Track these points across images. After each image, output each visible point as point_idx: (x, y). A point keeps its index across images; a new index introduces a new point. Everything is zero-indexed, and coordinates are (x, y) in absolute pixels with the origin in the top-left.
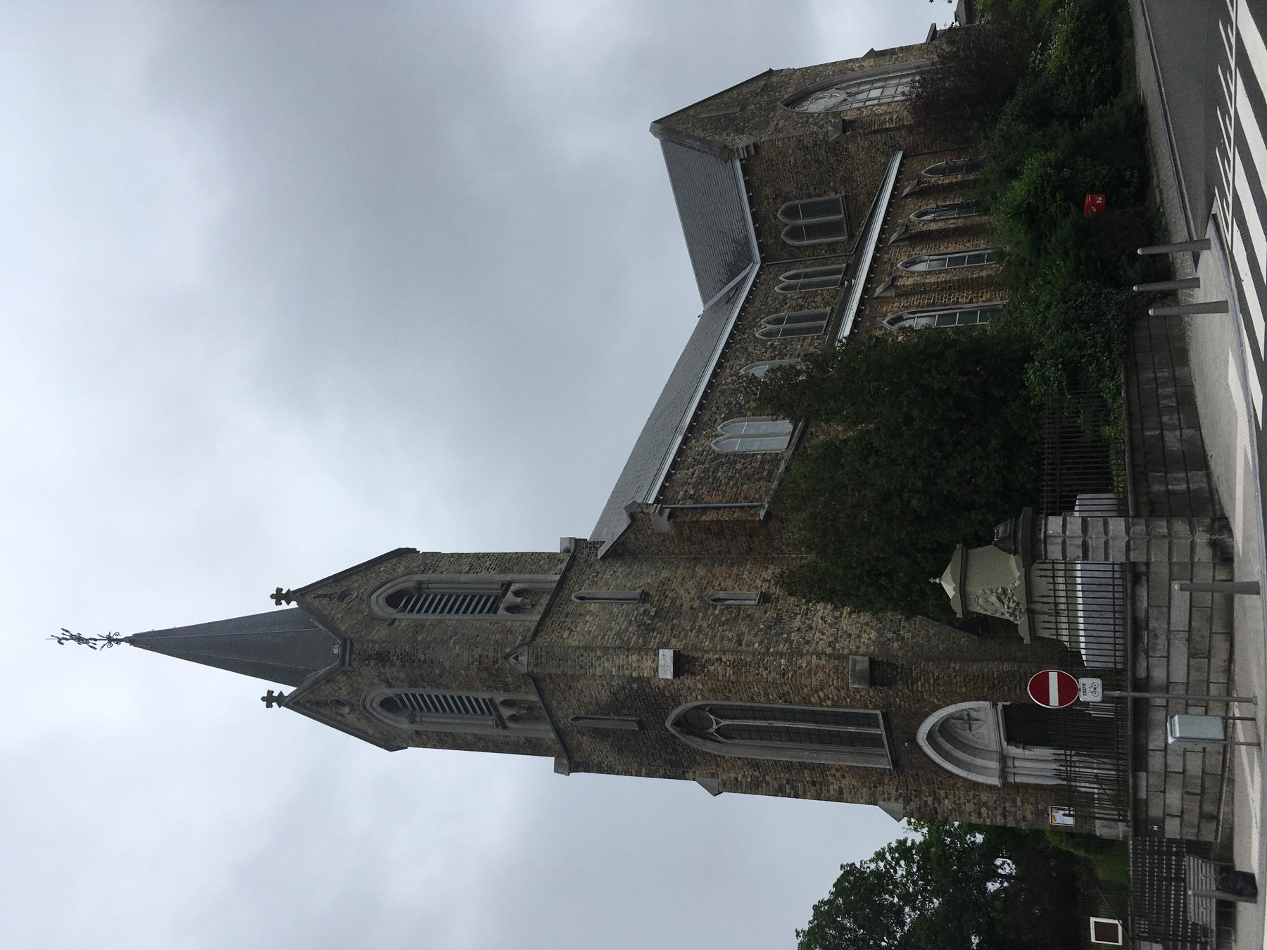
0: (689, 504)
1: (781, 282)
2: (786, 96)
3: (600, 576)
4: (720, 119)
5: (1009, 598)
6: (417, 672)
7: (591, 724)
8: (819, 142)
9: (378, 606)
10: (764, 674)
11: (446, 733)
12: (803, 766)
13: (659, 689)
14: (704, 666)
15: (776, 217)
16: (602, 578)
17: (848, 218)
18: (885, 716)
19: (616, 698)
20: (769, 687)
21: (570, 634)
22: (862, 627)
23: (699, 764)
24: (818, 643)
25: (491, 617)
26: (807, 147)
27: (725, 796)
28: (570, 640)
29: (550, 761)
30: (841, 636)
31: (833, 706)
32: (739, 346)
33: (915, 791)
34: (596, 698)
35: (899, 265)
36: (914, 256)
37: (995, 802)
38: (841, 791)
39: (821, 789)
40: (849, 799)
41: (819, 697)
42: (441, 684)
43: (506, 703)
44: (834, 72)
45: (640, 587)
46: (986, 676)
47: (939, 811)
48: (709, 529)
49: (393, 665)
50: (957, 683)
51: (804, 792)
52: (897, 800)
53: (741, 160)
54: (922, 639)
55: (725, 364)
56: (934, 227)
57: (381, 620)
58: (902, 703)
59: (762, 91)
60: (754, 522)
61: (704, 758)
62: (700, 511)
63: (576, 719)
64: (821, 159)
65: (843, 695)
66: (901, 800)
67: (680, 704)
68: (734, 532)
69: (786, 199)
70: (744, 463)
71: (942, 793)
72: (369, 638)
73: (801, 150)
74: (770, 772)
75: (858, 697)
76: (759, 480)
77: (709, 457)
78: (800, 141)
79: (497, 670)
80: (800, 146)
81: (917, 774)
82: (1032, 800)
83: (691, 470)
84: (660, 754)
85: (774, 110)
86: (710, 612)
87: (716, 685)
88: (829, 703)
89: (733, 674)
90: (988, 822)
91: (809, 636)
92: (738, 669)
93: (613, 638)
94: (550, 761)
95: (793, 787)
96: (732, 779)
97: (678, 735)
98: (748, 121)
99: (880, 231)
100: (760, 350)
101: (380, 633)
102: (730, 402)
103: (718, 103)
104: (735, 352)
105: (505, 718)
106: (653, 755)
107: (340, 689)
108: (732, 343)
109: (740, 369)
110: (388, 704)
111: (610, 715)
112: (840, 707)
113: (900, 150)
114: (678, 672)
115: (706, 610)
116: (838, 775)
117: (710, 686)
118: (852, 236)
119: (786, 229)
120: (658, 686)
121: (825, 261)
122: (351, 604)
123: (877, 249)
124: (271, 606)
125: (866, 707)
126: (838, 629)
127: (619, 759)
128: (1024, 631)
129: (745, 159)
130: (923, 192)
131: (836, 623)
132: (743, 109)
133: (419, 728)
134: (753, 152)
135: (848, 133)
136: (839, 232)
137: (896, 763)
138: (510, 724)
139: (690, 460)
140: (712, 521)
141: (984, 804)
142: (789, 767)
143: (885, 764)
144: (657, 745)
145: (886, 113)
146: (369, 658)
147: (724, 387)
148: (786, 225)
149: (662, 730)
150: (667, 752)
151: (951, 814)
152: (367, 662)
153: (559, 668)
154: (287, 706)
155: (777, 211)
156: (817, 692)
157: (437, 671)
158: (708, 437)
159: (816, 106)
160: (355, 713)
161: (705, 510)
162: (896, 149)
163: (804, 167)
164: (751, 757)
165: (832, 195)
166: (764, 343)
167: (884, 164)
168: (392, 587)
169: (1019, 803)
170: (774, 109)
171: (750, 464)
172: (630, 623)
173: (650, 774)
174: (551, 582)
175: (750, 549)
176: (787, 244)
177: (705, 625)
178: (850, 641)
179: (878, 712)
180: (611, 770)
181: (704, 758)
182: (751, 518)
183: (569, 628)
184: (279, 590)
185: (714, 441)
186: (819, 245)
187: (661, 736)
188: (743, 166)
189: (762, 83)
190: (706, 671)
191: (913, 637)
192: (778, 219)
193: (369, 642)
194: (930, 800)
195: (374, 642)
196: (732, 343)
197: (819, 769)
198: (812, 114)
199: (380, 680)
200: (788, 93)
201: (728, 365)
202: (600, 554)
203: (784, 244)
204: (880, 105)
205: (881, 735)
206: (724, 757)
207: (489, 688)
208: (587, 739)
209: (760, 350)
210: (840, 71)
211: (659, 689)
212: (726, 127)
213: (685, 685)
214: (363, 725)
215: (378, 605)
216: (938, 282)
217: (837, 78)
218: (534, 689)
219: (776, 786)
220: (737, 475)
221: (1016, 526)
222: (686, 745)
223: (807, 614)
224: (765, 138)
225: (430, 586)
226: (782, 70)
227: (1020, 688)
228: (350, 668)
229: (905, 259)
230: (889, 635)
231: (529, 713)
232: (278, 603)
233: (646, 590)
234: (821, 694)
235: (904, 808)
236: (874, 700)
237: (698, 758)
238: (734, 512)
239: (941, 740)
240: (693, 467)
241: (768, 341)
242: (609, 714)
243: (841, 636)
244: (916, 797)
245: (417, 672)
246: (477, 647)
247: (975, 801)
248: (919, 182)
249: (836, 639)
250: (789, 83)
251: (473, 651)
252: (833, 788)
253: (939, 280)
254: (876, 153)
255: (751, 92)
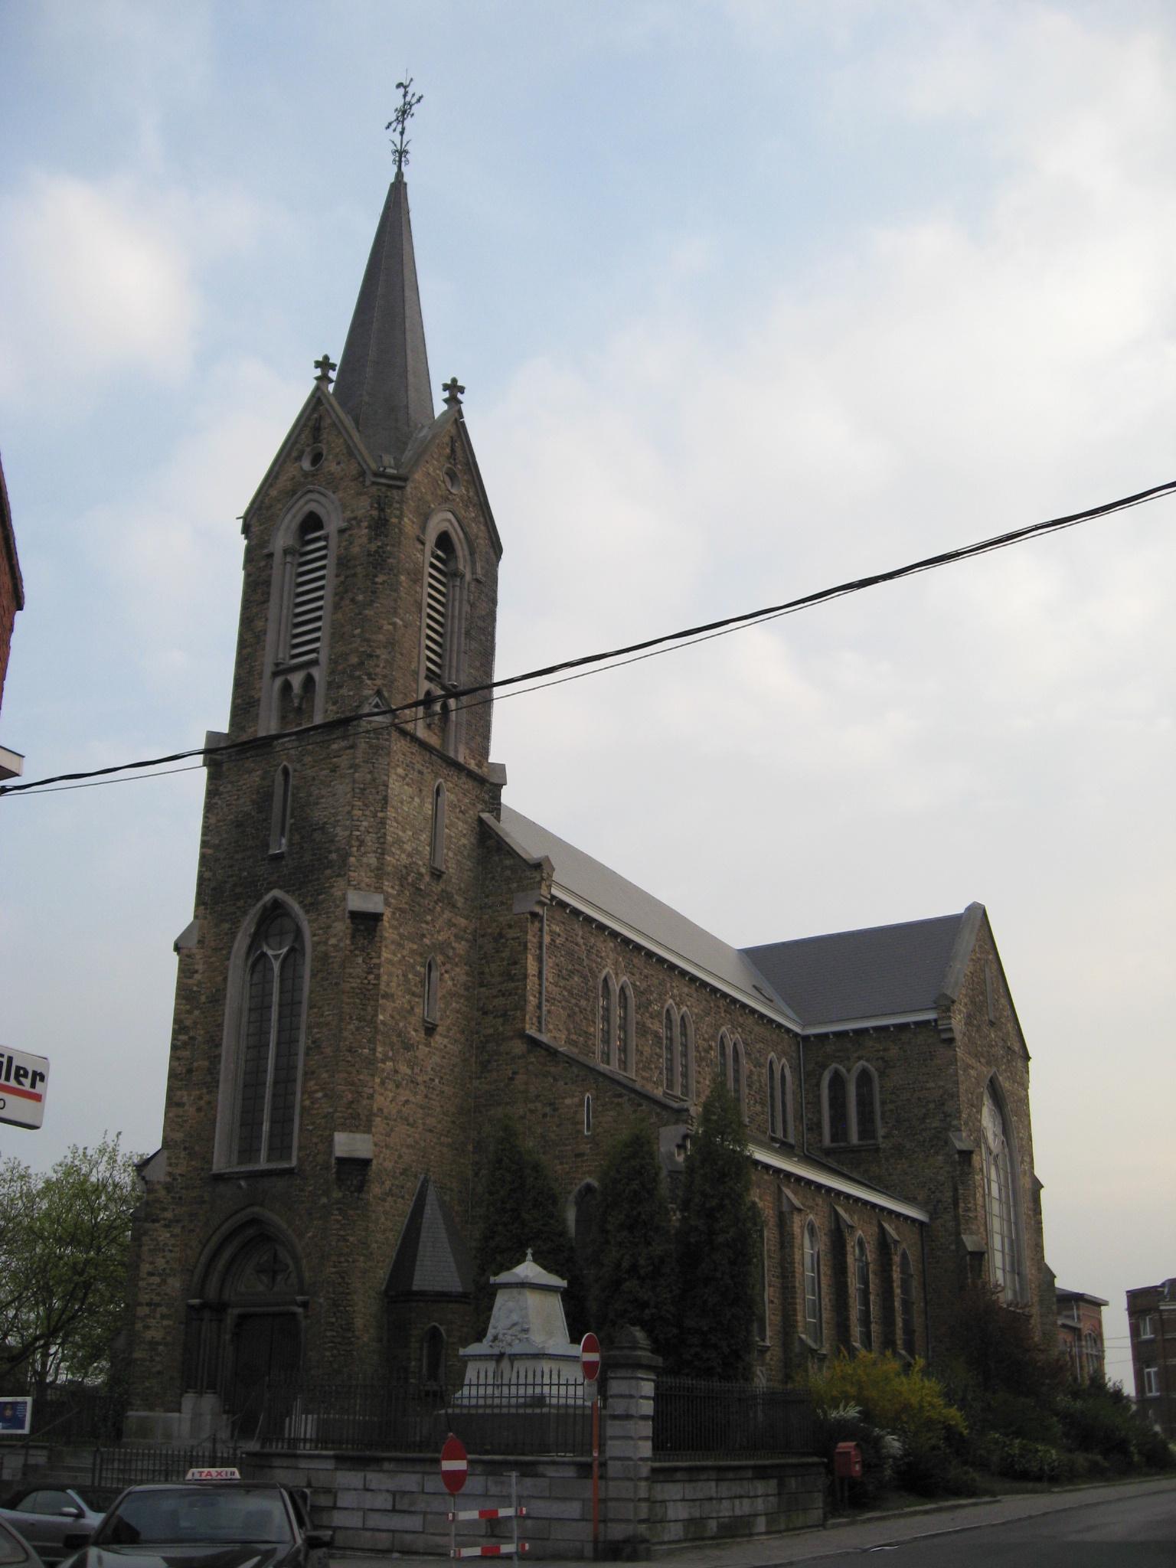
0: (547, 939)
1: (779, 1059)
2: (1000, 1078)
3: (461, 815)
4: (982, 993)
5: (516, 1336)
6: (359, 569)
7: (279, 791)
8: (948, 1119)
9: (441, 521)
10: (352, 1027)
11: (268, 593)
12: (215, 1060)
13: (329, 887)
14: (363, 949)
15: (860, 1058)
16: (458, 818)
17: (854, 1150)
18: (289, 1172)
19: (315, 830)
20: (330, 1030)
21: (400, 776)
22: (396, 1150)
23: (217, 926)
24: (382, 1094)
25: (423, 673)
26: (943, 1104)
27: (175, 958)
28: (395, 777)
29: (224, 727)
30: (388, 1124)
31: (303, 1108)
32: (712, 1005)
33: (180, 1198)
34: (317, 804)
35: (811, 1216)
36: (819, 1234)
37: (166, 1294)
38: (180, 1105)
39: (181, 1080)
40: (170, 1115)
41: (316, 1091)
42: (342, 599)
43: (309, 681)
44: (1022, 1139)
45: (447, 868)
46: (349, 1297)
47: (157, 1225)
48: (515, 963)
49: (370, 541)
50: (340, 1262)
51: (179, 1059)
52: (170, 1174)
53: (936, 1020)
54: (383, 1224)
55: (694, 986)
56: (850, 1259)
57: (423, 528)
58: (307, 1194)
59: (1008, 1048)
60: (523, 1020)
61: (227, 934)
62: (538, 952)
63: (286, 772)
64: (928, 1121)
65: (318, 1122)
66: (168, 1179)
67: (307, 912)
68: (510, 994)
69: (882, 1074)
70: (585, 1010)
71: (177, 1230)
72: (406, 511)
73: (941, 1097)
74: (206, 1017)
75: (315, 1140)
76: (568, 1029)
77: (594, 965)
78: (952, 1097)
79: (359, 677)
80: (946, 1097)
81: (204, 1202)
82: (169, 1339)
83: (581, 941)
84: (232, 876)
85: (987, 1063)
86: (419, 959)
87: (333, 963)
88: (307, 1103)
89: (352, 988)
90: (142, 1284)
91: (390, 1085)
92: (357, 994)
93: (395, 833)
94: (224, 727)
95: (185, 1044)
96: (196, 967)
97: (260, 905)
98: (979, 1029)
99: (789, 1172)
100: (706, 1032)
101: (409, 524)
102: (651, 993)
103: (999, 991)
104: (706, 1001)
105: (289, 678)
106: (231, 866)
107: (338, 463)
108: (716, 996)
109: (687, 1006)
110: (312, 523)
111: (291, 818)
112: (301, 1116)
113: (931, 1219)
114: (356, 916)
115: (421, 955)
116: (202, 1103)
117: (333, 954)
118: (828, 1152)
119: (843, 1070)
120: (333, 886)
121: (799, 1118)
122: (443, 485)
123: (830, 1190)
124: (438, 378)
125: (300, 1148)
126: (395, 1120)
127: (225, 820)
128: (474, 1349)
129: (936, 1025)
130: (884, 1245)
131: (401, 1118)
132: (992, 1024)
133: (278, 559)
134: (944, 1036)
135: (957, 1156)
136: (834, 1139)
137: (219, 1178)
138: (279, 682)
139: (593, 940)
140: (526, 969)
141: (164, 1281)
142: (215, 1042)
143: (219, 1165)
144: (246, 874)
145: (975, 1204)
146: (381, 510)
147: (669, 985)
148: (849, 1071)
149: (268, 883)
150: (235, 885)
151: (152, 1240)
152: (376, 505)
153: (364, 762)
154: (317, 389)
155: (868, 1060)
156: (322, 1089)
157: (360, 598)
158: (616, 963)
159: (988, 1119)
160: (303, 476)
161: (540, 960)
162: (933, 1215)
163: (919, 1099)
164: (228, 996)
165: (881, 1131)
166: (713, 1037)
167: (915, 1199)
168: (459, 539)
169: (165, 1323)
170: (988, 1063)
171: (585, 1018)
172: (410, 855)
173: (204, 860)
174: (456, 751)
175: (485, 1013)
176: (824, 1070)
177: (405, 953)
178: (382, 1134)
179: (294, 1163)
180: (209, 808)
181: (227, 934)
182: (527, 1017)
183: (407, 775)
184: (462, 390)
185: (611, 971)
186: (819, 1112)
187: (259, 880)
188: (928, 1022)
189: (1017, 1047)
190: (357, 952)
191: (385, 1213)
192: (857, 1062)
193: (401, 509)
194: (168, 1215)
195: (400, 517)
196: (716, 996)
197: (210, 1080)
198: (980, 1112)
199: (349, 520)
200: (1006, 1085)
201: (693, 991)
202: (485, 816)
203: (824, 1067)
204: (984, 1196)
205: (257, 1161)
206: (228, 959)
207: (333, 662)
208: (255, 782)
209: (706, 1032)
210: (1022, 1146)
211: (329, 887)
212: (973, 1002)
213: (333, 922)
214: (283, 482)
215: (438, 523)
216: (794, 1263)
217: (1015, 1142)
218: (332, 717)
219: (188, 1023)
220: (573, 1001)
221: (645, 1349)
222: (245, 913)
223: (412, 1082)
224: (960, 1052)
225: (457, 589)
226: (1028, 1072)
227: (334, 1337)
228: (368, 483)
229: (817, 1225)
230: (388, 1184)
231: (293, 705)
232: (446, 387)
233: (445, 876)
234: (320, 1095)
235: (159, 1182)
236: (311, 1159)
237: (226, 926)
238: (535, 997)
239: (251, 1232)
240: (585, 944)
241: (716, 1042)
242: (292, 816)
243: (388, 1124)
244: (173, 1198)
245: (359, 569)
246: (390, 653)
247: (168, 1271)
248: (896, 1242)
249: (386, 1118)
250: (1014, 1082)
251: (385, 647)
252: (184, 1096)
253: (796, 1265)
254: (930, 1189)
255: (1008, 1033)
